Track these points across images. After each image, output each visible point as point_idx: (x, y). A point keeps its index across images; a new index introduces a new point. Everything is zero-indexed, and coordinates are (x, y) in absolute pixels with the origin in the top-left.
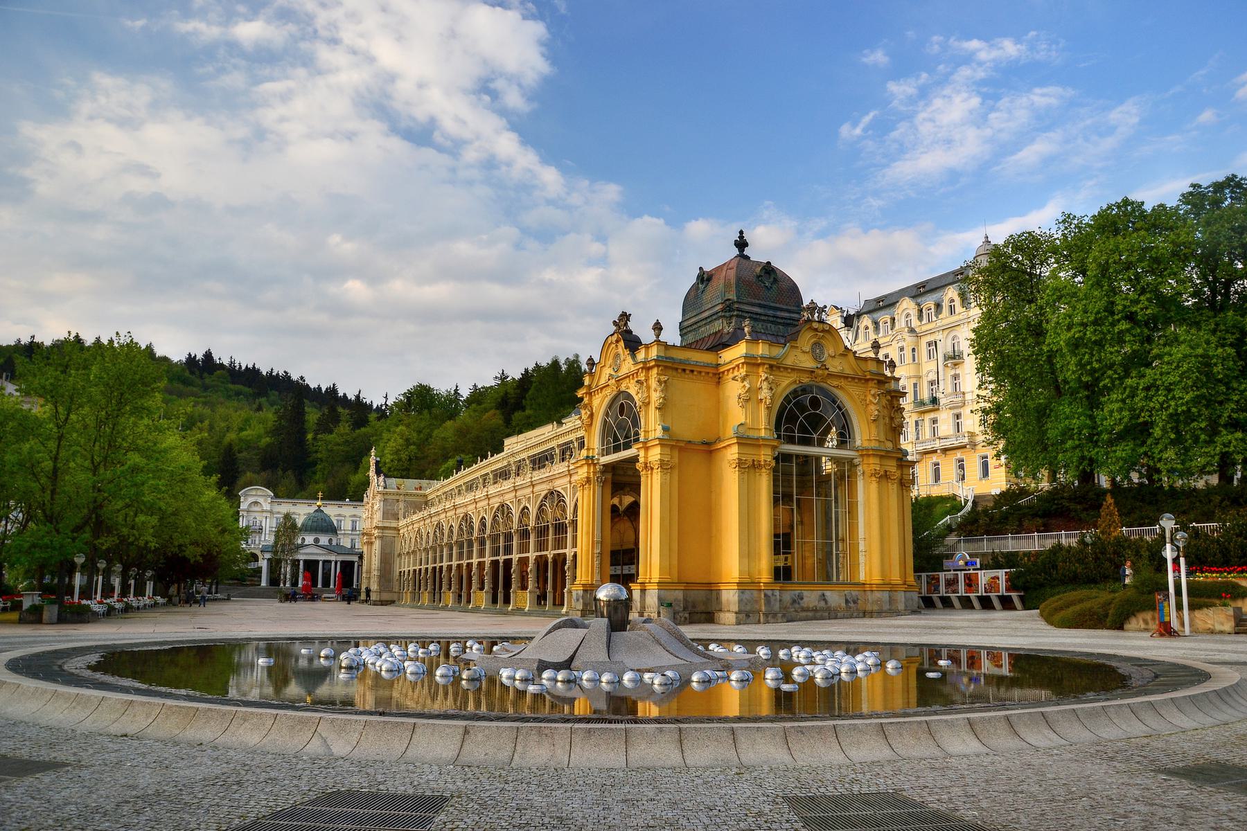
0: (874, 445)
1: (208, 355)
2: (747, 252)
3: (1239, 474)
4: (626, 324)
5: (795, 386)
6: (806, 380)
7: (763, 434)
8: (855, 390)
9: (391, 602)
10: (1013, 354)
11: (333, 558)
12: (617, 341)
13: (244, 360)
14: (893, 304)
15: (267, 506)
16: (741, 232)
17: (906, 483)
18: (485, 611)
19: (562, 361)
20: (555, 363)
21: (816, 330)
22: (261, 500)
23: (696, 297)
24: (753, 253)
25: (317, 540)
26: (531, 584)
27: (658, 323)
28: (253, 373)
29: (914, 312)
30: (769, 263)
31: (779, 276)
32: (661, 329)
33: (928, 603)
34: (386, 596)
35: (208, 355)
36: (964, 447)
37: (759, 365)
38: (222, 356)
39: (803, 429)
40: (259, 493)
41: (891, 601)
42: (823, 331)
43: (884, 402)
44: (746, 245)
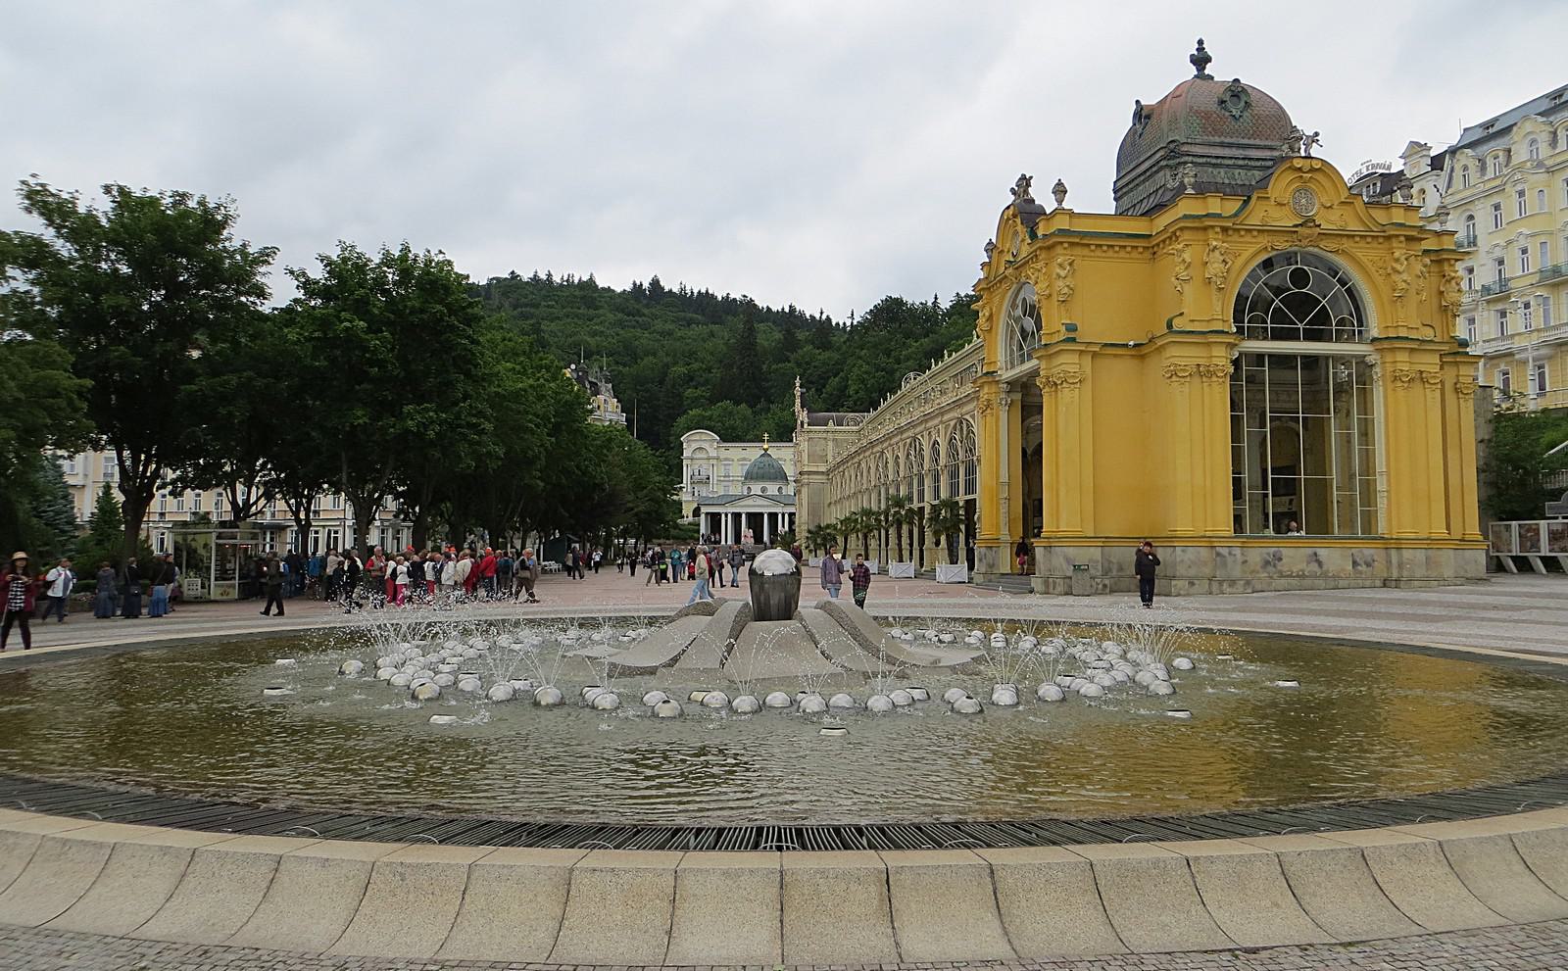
1: (655, 283)
4: (1026, 192)
6: (1283, 245)
8: (1368, 254)
13: (696, 285)
14: (1508, 130)
15: (713, 453)
16: (1201, 42)
23: (1133, 144)
24: (1220, 71)
25: (764, 490)
27: (1060, 184)
28: (706, 298)
29: (1544, 138)
31: (1254, 97)
33: (1497, 567)
35: (655, 283)
38: (670, 284)
39: (1279, 316)
42: (1312, 170)
44: (1208, 59)
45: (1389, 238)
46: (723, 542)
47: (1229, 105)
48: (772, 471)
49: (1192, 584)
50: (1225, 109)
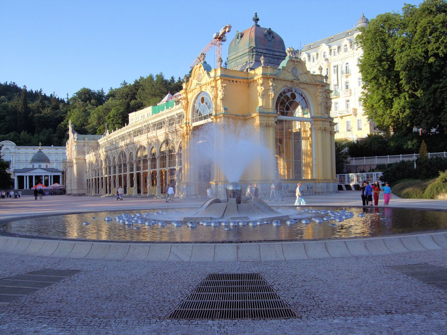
0: (319, 115)
2: (259, 23)
3: (37, 115)
5: (284, 88)
6: (289, 85)
7: (270, 111)
9: (84, 195)
10: (381, 70)
11: (49, 174)
12: (200, 67)
16: (256, 14)
17: (332, 133)
18: (135, 197)
19: (154, 76)
20: (151, 77)
21: (294, 61)
22: (9, 147)
25: (40, 166)
26: (158, 184)
27: (320, 67)
30: (270, 29)
32: (322, 69)
33: (340, 188)
34: (81, 192)
36: (351, 115)
37: (268, 78)
40: (8, 144)
41: (327, 187)
42: (297, 62)
43: (324, 95)
45: (317, 85)
46: (25, 188)
47: (268, 36)
48: (43, 158)
49: (265, 195)
50: (266, 37)
